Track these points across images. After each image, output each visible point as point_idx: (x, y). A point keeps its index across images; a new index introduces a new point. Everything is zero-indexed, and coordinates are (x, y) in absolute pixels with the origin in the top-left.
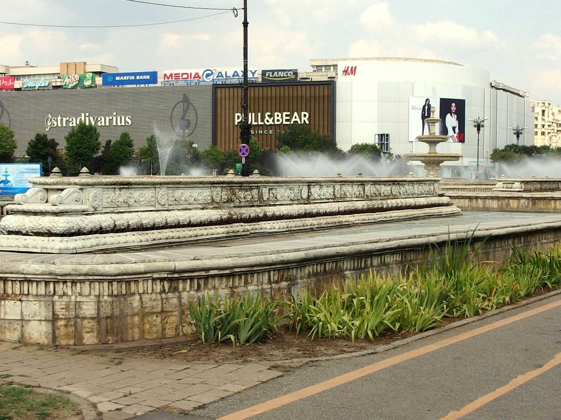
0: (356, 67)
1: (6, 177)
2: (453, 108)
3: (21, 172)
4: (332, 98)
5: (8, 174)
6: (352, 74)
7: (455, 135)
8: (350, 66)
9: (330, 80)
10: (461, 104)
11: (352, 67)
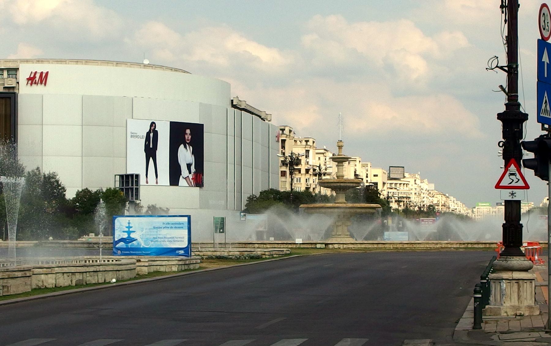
0: (47, 73)
1: (129, 234)
2: (188, 137)
3: (154, 228)
4: (12, 118)
5: (131, 229)
6: (41, 83)
7: (191, 176)
8: (39, 71)
9: (7, 91)
10: (198, 130)
11: (42, 73)
